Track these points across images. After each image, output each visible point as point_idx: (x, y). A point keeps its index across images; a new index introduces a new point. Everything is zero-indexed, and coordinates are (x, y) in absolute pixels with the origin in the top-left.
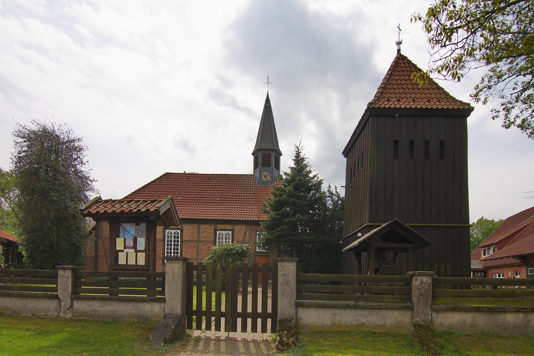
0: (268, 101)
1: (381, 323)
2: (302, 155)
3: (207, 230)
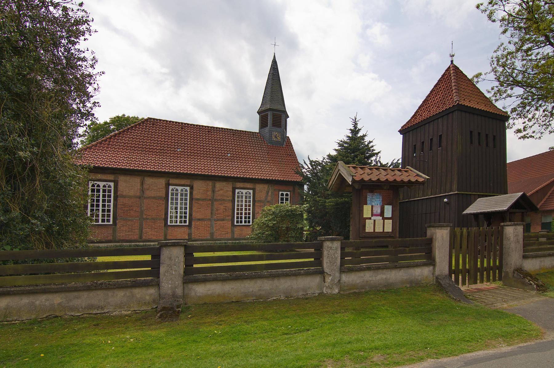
0: (274, 63)
2: (359, 127)
3: (155, 185)
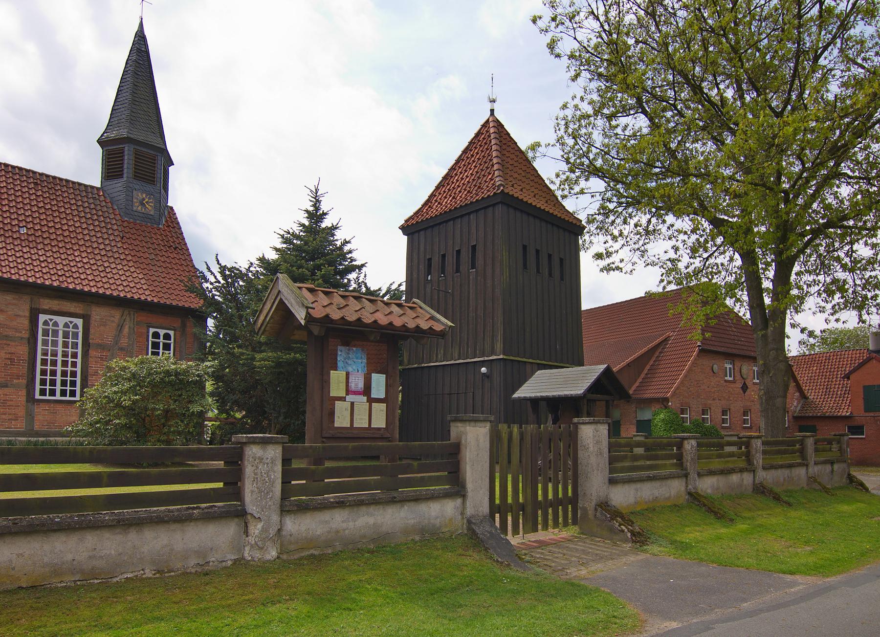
1: (667, 495)
